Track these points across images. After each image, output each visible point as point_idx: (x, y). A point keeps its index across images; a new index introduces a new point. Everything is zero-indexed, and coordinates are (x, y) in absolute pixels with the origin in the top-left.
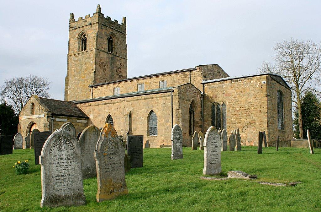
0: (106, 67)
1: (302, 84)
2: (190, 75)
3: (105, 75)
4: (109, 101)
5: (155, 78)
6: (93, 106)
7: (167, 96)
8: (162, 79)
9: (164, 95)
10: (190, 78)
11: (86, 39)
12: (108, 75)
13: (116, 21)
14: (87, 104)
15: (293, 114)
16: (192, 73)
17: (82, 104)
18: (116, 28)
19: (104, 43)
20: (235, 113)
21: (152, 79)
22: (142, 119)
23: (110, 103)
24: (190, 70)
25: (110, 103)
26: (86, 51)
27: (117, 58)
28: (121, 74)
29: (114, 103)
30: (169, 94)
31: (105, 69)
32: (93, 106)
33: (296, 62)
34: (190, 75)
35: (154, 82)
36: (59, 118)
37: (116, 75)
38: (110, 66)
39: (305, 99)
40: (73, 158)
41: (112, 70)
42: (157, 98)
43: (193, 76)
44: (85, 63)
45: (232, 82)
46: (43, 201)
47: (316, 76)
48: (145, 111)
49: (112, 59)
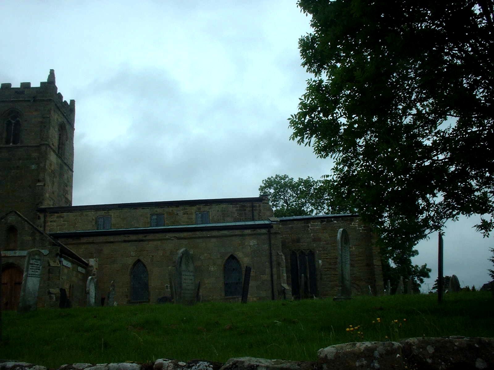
4: (141, 237)
7: (260, 234)
8: (199, 209)
9: (253, 233)
10: (253, 213)
11: (18, 124)
13: (315, 75)
14: (84, 240)
17: (70, 241)
20: (330, 266)
21: (181, 208)
22: (212, 269)
23: (142, 241)
29: (149, 240)
30: (264, 231)
35: (184, 214)
42: (241, 235)
43: (258, 208)
44: (18, 167)
45: (322, 222)
48: (219, 256)
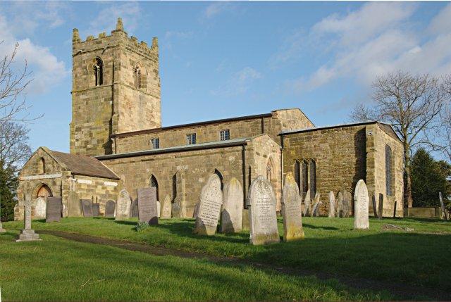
0: (132, 110)
1: (412, 136)
2: (262, 122)
3: (132, 120)
4: (151, 157)
5: (212, 126)
6: (126, 163)
12: (136, 121)
15: (443, 204)
16: (266, 120)
18: (145, 54)
19: (129, 75)
21: (208, 127)
23: (152, 160)
24: (262, 117)
25: (152, 160)
26: (102, 85)
27: (147, 96)
28: (152, 120)
30: (240, 148)
31: (131, 113)
32: (126, 163)
33: (405, 105)
34: (262, 122)
36: (82, 178)
37: (146, 121)
38: (137, 108)
39: (415, 163)
40: (270, 202)
41: (140, 114)
46: (396, 184)
47: (433, 125)
49: (141, 98)
